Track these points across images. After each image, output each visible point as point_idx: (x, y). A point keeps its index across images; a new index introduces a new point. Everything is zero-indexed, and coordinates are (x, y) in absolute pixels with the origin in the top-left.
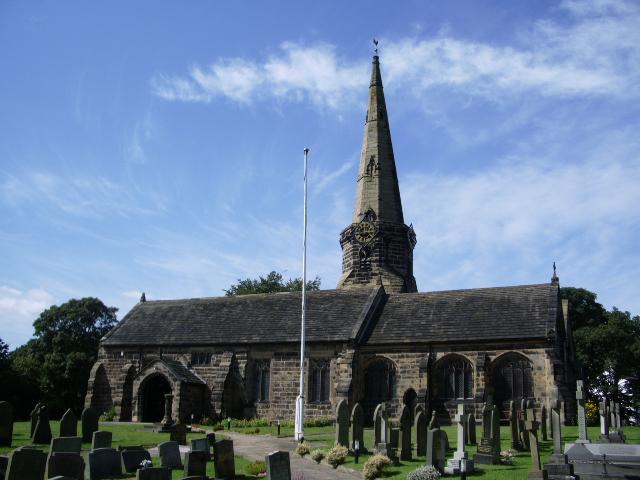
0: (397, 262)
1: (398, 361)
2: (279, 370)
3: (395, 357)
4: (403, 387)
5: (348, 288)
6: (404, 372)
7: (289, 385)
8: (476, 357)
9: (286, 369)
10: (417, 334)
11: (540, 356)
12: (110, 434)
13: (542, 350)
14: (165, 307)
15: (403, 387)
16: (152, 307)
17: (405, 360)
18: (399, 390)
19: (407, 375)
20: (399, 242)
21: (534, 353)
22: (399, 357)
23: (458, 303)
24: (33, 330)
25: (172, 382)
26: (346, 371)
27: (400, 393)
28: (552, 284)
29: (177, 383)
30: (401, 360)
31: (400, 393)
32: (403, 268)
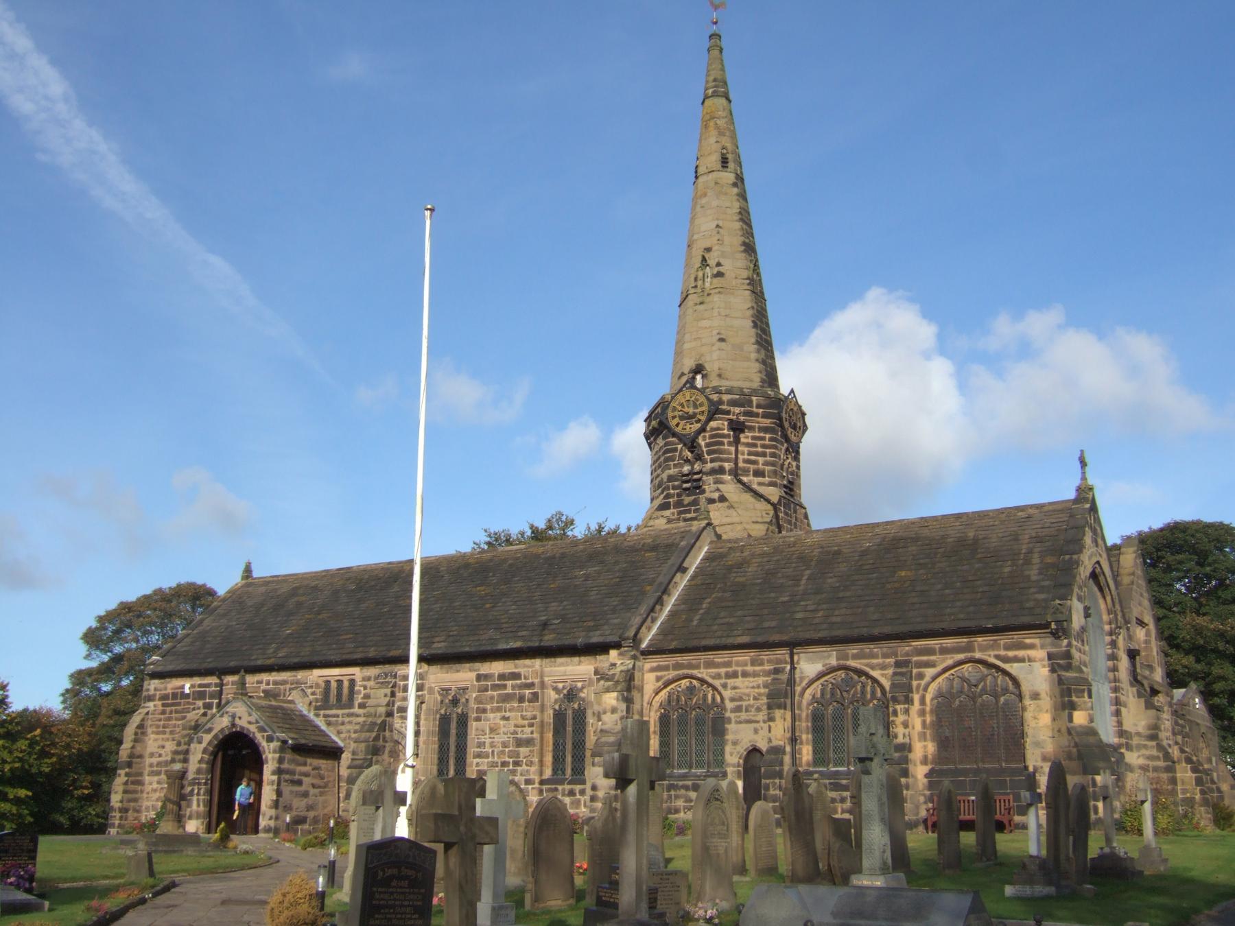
0: (758, 473)
1: (725, 686)
2: (484, 711)
3: (718, 676)
4: (735, 743)
5: (660, 523)
6: (738, 709)
7: (505, 745)
8: (890, 671)
9: (499, 709)
10: (766, 624)
11: (1036, 665)
12: (496, 819)
13: (146, 683)
14: (284, 589)
15: (735, 743)
16: (262, 589)
17: (738, 682)
18: (728, 749)
19: (744, 716)
20: (761, 429)
21: (1022, 660)
22: (728, 676)
23: (864, 553)
24: (83, 648)
25: (264, 744)
26: (614, 710)
27: (733, 757)
28: (1076, 501)
29: (275, 745)
30: (731, 682)
31: (733, 757)
32: (772, 484)
